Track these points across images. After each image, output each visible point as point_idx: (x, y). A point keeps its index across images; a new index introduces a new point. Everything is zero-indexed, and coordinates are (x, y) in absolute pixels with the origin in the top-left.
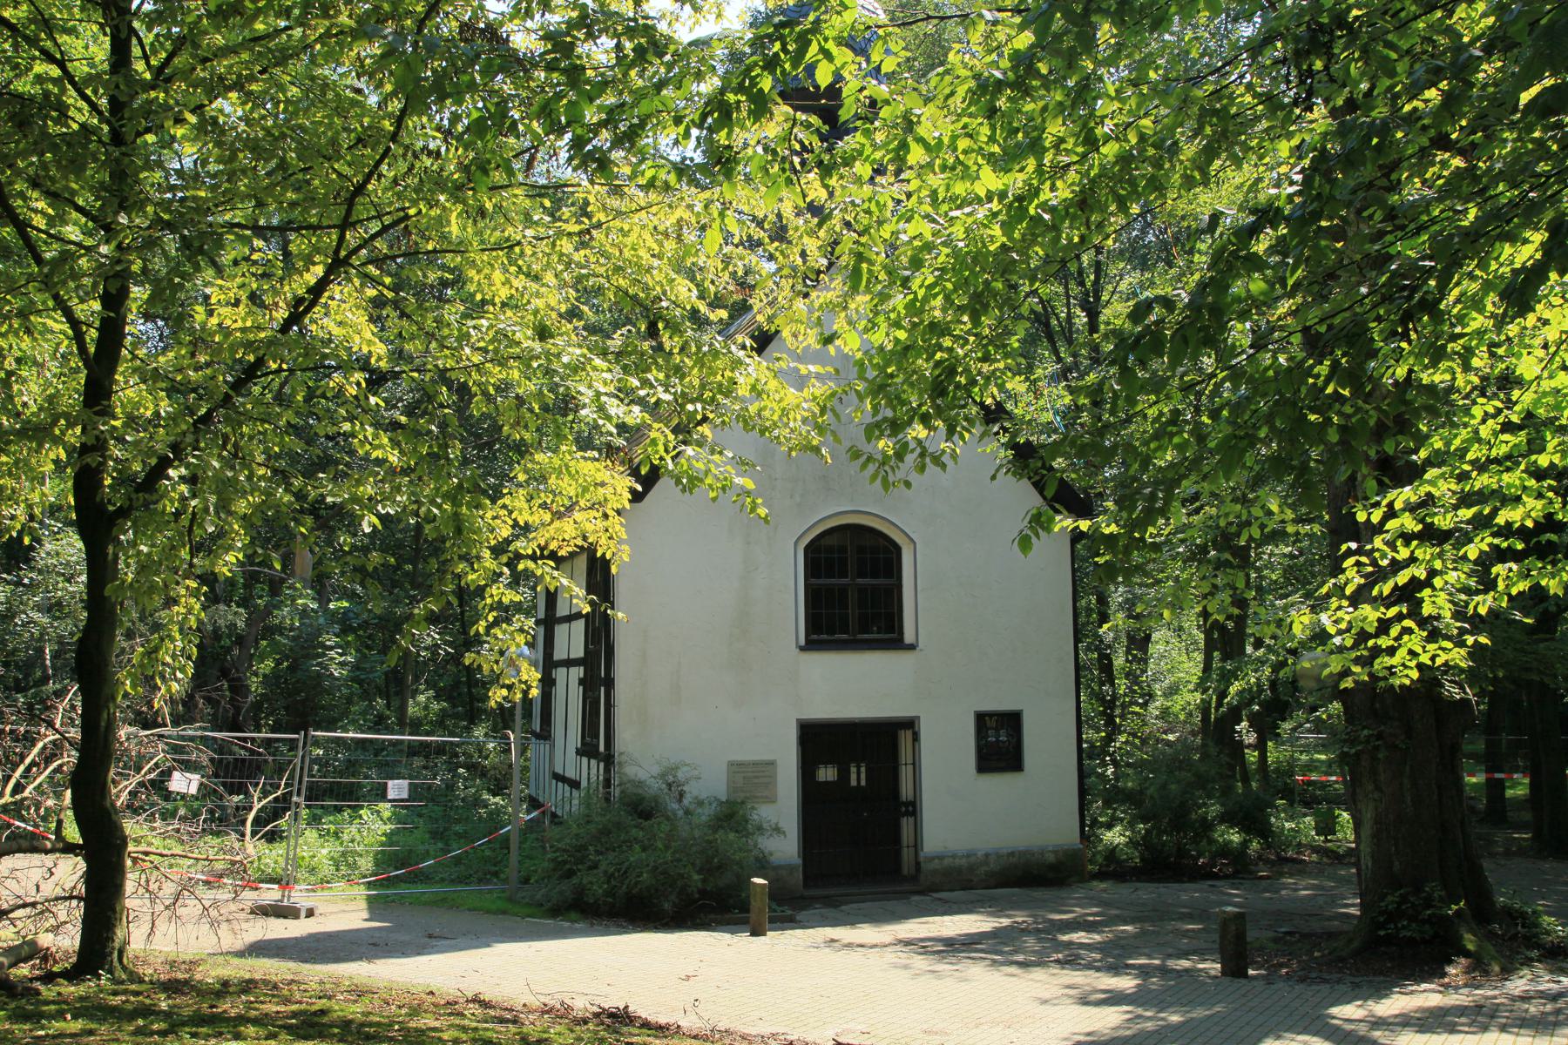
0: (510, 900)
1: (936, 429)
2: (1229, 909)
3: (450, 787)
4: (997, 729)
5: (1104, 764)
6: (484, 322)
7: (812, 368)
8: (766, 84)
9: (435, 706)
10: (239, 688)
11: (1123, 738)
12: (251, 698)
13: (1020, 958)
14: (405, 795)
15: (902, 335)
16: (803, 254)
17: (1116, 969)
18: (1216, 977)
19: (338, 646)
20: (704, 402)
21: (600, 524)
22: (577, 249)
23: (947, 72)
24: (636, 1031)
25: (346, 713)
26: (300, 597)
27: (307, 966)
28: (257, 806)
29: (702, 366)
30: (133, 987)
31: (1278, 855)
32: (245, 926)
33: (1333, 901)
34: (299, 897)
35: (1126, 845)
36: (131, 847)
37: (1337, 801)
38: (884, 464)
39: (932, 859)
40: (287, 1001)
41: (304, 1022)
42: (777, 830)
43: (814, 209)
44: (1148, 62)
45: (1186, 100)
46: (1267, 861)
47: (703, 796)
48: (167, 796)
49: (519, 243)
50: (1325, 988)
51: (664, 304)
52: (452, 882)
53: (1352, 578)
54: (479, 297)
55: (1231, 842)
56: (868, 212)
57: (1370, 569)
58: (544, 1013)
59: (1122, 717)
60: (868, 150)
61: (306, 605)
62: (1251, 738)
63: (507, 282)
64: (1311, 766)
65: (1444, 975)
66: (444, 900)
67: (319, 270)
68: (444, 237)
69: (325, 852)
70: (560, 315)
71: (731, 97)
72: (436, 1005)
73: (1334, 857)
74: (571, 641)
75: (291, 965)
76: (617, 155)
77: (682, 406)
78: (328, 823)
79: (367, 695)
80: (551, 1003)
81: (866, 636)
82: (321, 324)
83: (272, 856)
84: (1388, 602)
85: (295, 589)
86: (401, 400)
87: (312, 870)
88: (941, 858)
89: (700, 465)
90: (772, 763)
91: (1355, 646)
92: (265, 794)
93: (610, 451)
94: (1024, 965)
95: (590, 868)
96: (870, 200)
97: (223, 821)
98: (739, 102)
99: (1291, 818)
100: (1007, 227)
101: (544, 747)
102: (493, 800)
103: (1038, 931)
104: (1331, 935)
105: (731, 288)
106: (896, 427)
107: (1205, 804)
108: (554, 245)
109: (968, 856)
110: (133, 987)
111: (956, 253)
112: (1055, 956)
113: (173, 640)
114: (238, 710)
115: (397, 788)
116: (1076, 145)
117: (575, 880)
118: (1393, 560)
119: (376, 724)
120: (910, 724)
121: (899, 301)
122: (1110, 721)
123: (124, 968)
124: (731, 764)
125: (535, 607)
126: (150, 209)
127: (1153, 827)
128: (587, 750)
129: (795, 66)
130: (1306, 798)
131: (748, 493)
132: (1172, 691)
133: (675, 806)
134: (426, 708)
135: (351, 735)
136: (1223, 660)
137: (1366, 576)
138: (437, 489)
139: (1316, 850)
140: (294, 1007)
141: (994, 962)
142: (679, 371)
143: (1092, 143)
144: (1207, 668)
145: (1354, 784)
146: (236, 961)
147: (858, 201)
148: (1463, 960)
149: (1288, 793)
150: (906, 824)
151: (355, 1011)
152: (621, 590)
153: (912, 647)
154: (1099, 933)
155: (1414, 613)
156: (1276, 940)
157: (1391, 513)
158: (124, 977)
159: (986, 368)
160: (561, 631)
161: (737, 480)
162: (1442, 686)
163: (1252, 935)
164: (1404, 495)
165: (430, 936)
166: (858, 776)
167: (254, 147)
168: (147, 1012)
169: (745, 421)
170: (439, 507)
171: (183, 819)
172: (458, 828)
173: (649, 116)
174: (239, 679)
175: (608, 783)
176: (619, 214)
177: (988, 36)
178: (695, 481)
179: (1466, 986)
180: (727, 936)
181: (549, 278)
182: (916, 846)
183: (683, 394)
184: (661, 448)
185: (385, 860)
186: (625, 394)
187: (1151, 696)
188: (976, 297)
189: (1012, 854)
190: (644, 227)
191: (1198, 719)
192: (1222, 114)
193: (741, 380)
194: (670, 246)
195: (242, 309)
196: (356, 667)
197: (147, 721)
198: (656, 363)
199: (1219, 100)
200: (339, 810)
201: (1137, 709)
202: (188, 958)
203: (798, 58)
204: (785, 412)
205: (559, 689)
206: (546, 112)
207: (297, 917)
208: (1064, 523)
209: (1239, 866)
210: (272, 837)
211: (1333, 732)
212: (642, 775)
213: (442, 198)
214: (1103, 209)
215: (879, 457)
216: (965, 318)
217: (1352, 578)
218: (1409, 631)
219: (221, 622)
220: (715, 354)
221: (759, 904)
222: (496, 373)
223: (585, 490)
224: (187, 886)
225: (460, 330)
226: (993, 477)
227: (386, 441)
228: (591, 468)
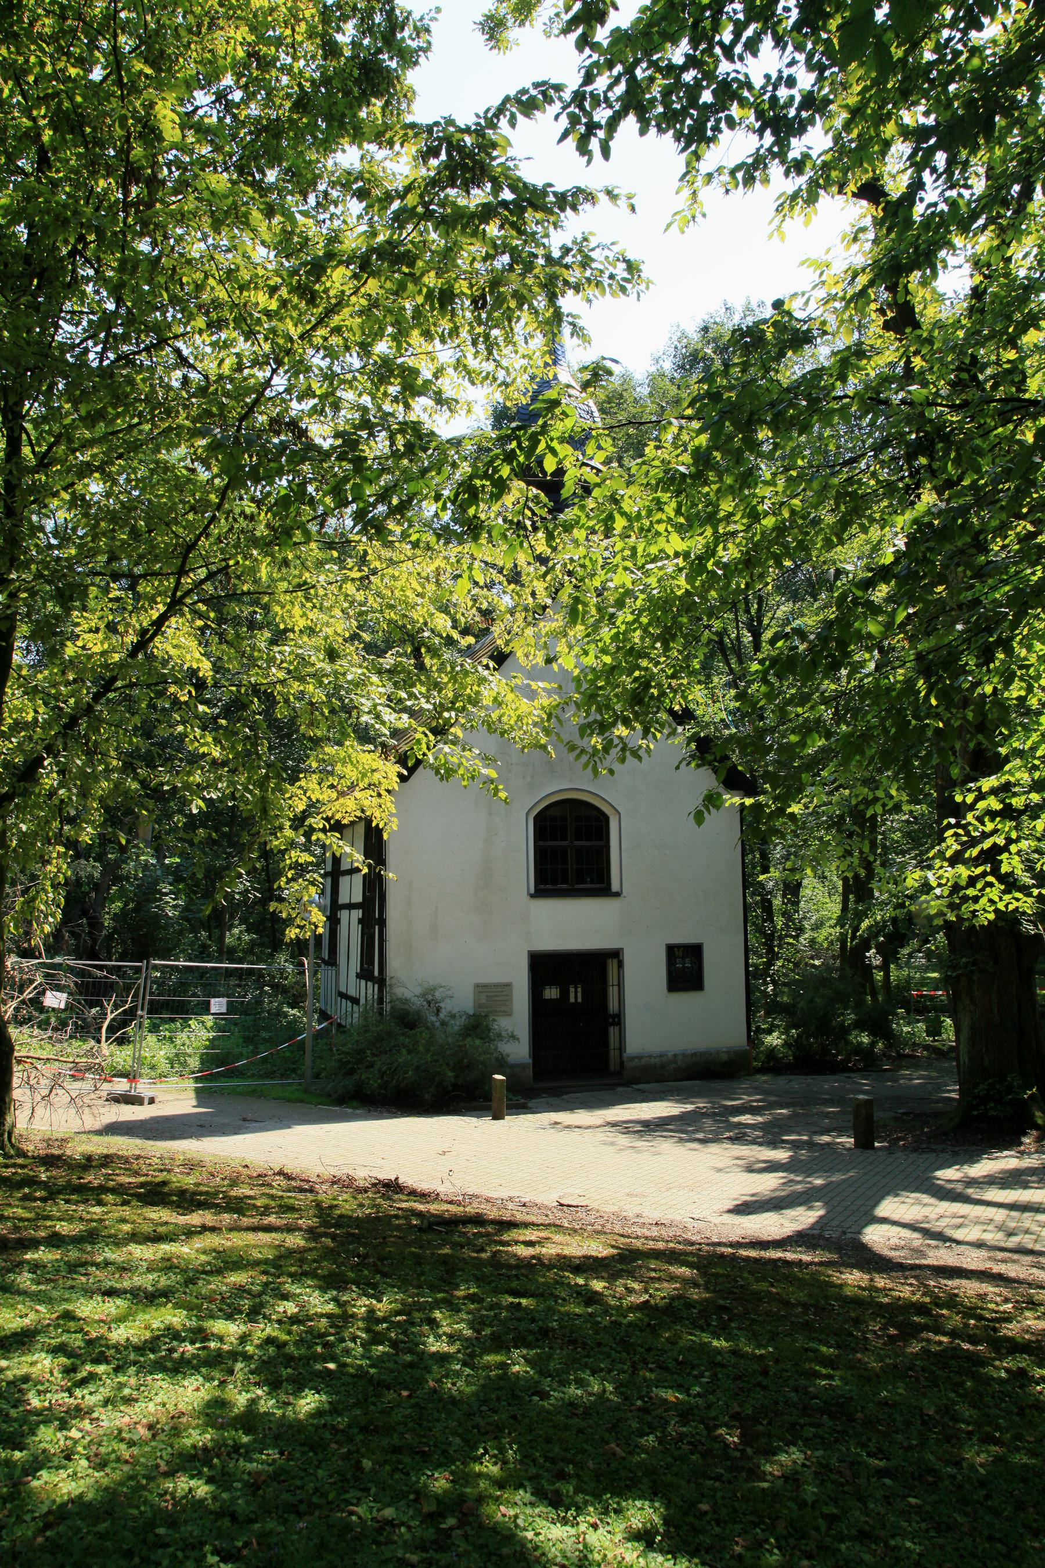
0: (306, 1091)
1: (634, 729)
2: (861, 1097)
3: (258, 1002)
4: (683, 958)
5: (765, 983)
6: (287, 648)
7: (540, 684)
8: (505, 471)
9: (246, 937)
10: (95, 924)
11: (779, 963)
12: (105, 932)
13: (700, 1136)
14: (224, 1010)
15: (607, 659)
16: (533, 594)
17: (774, 1143)
18: (850, 1149)
19: (171, 892)
20: (457, 710)
21: (376, 801)
22: (358, 590)
23: (644, 463)
24: (405, 1198)
25: (177, 945)
26: (143, 854)
27: (151, 1143)
28: (110, 1017)
29: (456, 681)
30: (20, 1161)
31: (898, 1052)
32: (102, 1110)
33: (939, 1088)
34: (143, 1088)
35: (783, 1046)
36: (16, 1054)
37: (942, 1010)
38: (594, 755)
39: (632, 1059)
40: (136, 1173)
41: (150, 1191)
42: (513, 1037)
43: (542, 560)
44: (797, 452)
45: (826, 487)
46: (889, 1057)
47: (455, 1011)
48: (42, 1009)
49: (314, 587)
50: (932, 1156)
51: (426, 634)
52: (261, 1077)
53: (951, 845)
54: (282, 626)
55: (862, 1043)
56: (583, 566)
57: (965, 839)
58: (334, 1183)
59: (780, 947)
60: (584, 519)
61: (147, 861)
62: (877, 961)
63: (304, 615)
64: (923, 983)
65: (1021, 1144)
66: (254, 1091)
67: (162, 608)
68: (256, 581)
69: (162, 1053)
70: (345, 640)
71: (478, 482)
72: (250, 1177)
73: (940, 1054)
74: (352, 890)
75: (138, 1142)
76: (391, 525)
77: (440, 714)
78: (165, 1032)
79: (194, 930)
80: (338, 1174)
81: (582, 886)
82: (160, 646)
83: (122, 1056)
84: (976, 861)
85: (139, 848)
86: (220, 700)
87: (153, 1067)
88: (639, 1057)
89: (455, 760)
90: (509, 985)
91: (951, 894)
92: (116, 1007)
93: (385, 750)
94: (703, 1141)
95: (368, 1067)
96: (585, 557)
97: (87, 1030)
98: (483, 486)
99: (909, 1024)
100: (690, 579)
101: (331, 972)
102: (292, 1012)
103: (715, 1114)
104: (937, 1115)
105: (477, 619)
106: (603, 727)
107: (843, 1014)
108: (341, 587)
109: (661, 1056)
110: (20, 1161)
111: (650, 598)
112: (727, 1134)
113: (46, 892)
114: (95, 941)
115: (218, 1005)
116: (742, 517)
117: (356, 1077)
118: (983, 832)
119: (202, 953)
120: (616, 955)
121: (606, 633)
122: (770, 950)
123: (13, 1146)
124: (477, 986)
125: (324, 861)
126: (33, 567)
127: (803, 1033)
128: (365, 974)
129: (527, 458)
130: (918, 1008)
131: (492, 781)
132: (818, 926)
133: (434, 1019)
134: (239, 939)
135: (182, 963)
136: (857, 902)
137: (962, 844)
138: (249, 778)
139: (927, 1047)
140: (142, 1179)
141: (681, 1140)
142: (437, 686)
143: (754, 516)
144: (845, 909)
145: (955, 999)
146: (96, 1139)
147: (576, 558)
148: (1034, 1132)
149: (906, 1003)
150: (613, 1032)
151: (189, 1181)
152: (392, 854)
153: (618, 894)
154: (761, 1115)
155: (995, 872)
156: (896, 1119)
157: (981, 796)
158: (12, 1152)
159: (674, 682)
160: (344, 881)
161: (483, 771)
162: (1021, 924)
163: (877, 1115)
164: (988, 783)
165: (244, 1120)
166: (575, 995)
167: (113, 517)
168: (32, 1182)
169: (489, 725)
170: (251, 792)
171: (55, 1029)
172: (264, 1034)
173: (415, 494)
174: (95, 918)
175: (381, 1001)
176: (392, 562)
177: (677, 437)
178: (450, 772)
179: (1037, 1152)
180: (474, 1119)
181: (337, 612)
182: (620, 1049)
183: (441, 705)
184: (424, 746)
185: (208, 1060)
186: (396, 705)
187: (801, 930)
188: (667, 630)
189: (695, 1054)
190: (410, 574)
191: (837, 946)
192: (853, 495)
193: (485, 693)
194: (431, 588)
195: (101, 635)
196: (186, 909)
197: (27, 953)
198: (420, 680)
199: (852, 485)
200: (173, 1020)
201: (791, 941)
202: (60, 1136)
203: (530, 452)
204: (520, 718)
205: (343, 927)
206: (337, 491)
207: (141, 1103)
208: (732, 800)
209: (868, 1061)
210: (122, 1041)
211: (939, 957)
212: (408, 994)
213: (255, 552)
214: (763, 564)
215: (591, 751)
216: (658, 645)
217: (951, 845)
218: (990, 885)
219: (82, 873)
220: (466, 673)
221: (500, 1096)
222: (296, 686)
223: (364, 775)
224: (56, 1083)
225: (268, 654)
226: (677, 768)
227: (210, 739)
228: (367, 758)
